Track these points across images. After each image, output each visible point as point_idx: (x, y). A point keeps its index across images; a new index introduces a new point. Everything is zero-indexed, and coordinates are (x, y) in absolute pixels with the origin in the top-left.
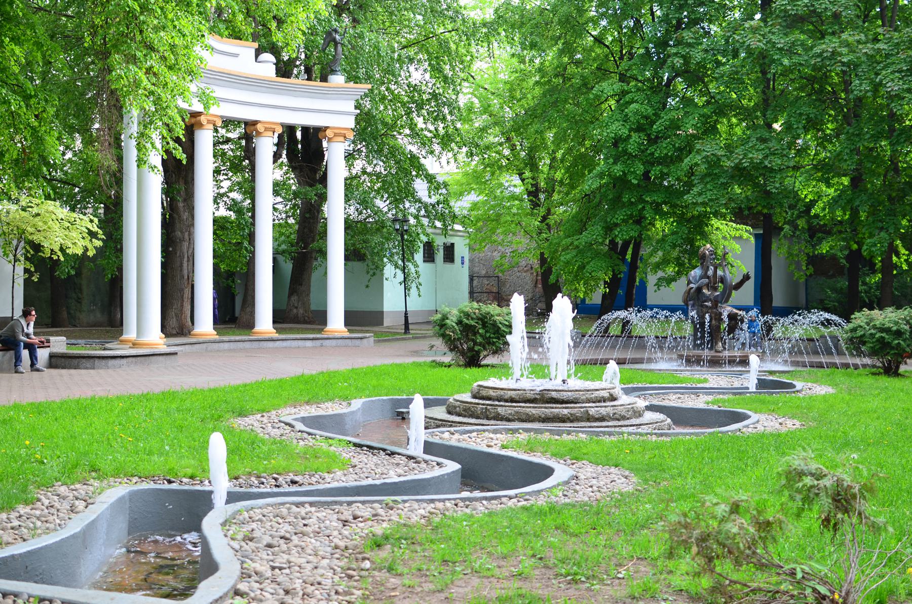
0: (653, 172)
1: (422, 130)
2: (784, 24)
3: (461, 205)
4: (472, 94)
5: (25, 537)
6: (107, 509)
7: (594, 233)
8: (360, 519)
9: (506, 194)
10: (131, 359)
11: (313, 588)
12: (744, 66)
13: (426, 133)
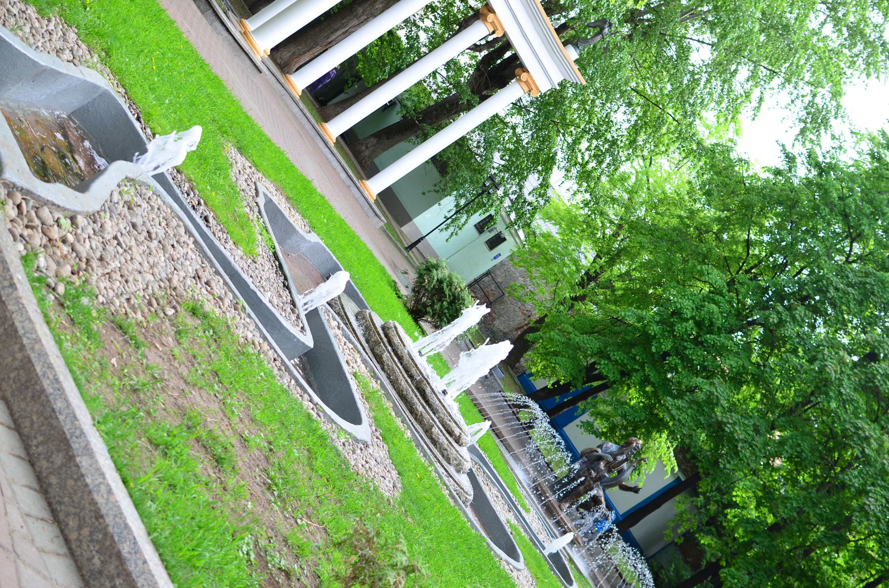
0: (671, 359)
1: (580, 151)
2: (863, 382)
3: (541, 224)
4: (637, 172)
5: (7, 24)
6: (79, 79)
7: (592, 343)
8: (209, 288)
9: (575, 255)
10: (231, 38)
11: (119, 278)
12: (806, 373)
13: (580, 156)
